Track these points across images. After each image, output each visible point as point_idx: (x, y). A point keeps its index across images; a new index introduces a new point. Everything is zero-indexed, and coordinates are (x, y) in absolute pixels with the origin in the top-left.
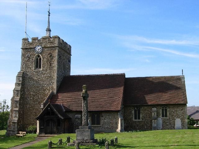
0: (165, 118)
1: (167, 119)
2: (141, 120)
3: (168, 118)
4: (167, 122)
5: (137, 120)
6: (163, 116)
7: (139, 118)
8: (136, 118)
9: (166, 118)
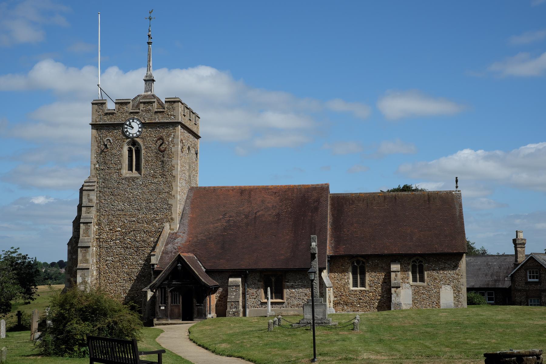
0: (418, 283)
1: (424, 287)
2: (367, 288)
3: (425, 284)
4: (422, 293)
5: (359, 288)
6: (414, 280)
7: (363, 285)
8: (355, 285)
9: (421, 284)
